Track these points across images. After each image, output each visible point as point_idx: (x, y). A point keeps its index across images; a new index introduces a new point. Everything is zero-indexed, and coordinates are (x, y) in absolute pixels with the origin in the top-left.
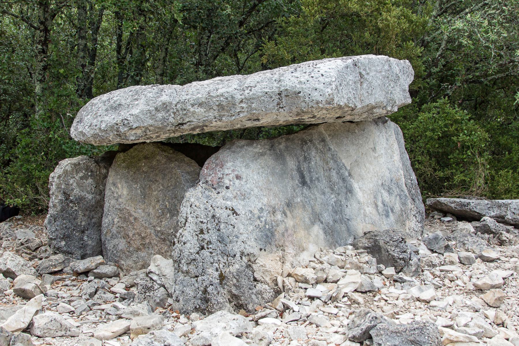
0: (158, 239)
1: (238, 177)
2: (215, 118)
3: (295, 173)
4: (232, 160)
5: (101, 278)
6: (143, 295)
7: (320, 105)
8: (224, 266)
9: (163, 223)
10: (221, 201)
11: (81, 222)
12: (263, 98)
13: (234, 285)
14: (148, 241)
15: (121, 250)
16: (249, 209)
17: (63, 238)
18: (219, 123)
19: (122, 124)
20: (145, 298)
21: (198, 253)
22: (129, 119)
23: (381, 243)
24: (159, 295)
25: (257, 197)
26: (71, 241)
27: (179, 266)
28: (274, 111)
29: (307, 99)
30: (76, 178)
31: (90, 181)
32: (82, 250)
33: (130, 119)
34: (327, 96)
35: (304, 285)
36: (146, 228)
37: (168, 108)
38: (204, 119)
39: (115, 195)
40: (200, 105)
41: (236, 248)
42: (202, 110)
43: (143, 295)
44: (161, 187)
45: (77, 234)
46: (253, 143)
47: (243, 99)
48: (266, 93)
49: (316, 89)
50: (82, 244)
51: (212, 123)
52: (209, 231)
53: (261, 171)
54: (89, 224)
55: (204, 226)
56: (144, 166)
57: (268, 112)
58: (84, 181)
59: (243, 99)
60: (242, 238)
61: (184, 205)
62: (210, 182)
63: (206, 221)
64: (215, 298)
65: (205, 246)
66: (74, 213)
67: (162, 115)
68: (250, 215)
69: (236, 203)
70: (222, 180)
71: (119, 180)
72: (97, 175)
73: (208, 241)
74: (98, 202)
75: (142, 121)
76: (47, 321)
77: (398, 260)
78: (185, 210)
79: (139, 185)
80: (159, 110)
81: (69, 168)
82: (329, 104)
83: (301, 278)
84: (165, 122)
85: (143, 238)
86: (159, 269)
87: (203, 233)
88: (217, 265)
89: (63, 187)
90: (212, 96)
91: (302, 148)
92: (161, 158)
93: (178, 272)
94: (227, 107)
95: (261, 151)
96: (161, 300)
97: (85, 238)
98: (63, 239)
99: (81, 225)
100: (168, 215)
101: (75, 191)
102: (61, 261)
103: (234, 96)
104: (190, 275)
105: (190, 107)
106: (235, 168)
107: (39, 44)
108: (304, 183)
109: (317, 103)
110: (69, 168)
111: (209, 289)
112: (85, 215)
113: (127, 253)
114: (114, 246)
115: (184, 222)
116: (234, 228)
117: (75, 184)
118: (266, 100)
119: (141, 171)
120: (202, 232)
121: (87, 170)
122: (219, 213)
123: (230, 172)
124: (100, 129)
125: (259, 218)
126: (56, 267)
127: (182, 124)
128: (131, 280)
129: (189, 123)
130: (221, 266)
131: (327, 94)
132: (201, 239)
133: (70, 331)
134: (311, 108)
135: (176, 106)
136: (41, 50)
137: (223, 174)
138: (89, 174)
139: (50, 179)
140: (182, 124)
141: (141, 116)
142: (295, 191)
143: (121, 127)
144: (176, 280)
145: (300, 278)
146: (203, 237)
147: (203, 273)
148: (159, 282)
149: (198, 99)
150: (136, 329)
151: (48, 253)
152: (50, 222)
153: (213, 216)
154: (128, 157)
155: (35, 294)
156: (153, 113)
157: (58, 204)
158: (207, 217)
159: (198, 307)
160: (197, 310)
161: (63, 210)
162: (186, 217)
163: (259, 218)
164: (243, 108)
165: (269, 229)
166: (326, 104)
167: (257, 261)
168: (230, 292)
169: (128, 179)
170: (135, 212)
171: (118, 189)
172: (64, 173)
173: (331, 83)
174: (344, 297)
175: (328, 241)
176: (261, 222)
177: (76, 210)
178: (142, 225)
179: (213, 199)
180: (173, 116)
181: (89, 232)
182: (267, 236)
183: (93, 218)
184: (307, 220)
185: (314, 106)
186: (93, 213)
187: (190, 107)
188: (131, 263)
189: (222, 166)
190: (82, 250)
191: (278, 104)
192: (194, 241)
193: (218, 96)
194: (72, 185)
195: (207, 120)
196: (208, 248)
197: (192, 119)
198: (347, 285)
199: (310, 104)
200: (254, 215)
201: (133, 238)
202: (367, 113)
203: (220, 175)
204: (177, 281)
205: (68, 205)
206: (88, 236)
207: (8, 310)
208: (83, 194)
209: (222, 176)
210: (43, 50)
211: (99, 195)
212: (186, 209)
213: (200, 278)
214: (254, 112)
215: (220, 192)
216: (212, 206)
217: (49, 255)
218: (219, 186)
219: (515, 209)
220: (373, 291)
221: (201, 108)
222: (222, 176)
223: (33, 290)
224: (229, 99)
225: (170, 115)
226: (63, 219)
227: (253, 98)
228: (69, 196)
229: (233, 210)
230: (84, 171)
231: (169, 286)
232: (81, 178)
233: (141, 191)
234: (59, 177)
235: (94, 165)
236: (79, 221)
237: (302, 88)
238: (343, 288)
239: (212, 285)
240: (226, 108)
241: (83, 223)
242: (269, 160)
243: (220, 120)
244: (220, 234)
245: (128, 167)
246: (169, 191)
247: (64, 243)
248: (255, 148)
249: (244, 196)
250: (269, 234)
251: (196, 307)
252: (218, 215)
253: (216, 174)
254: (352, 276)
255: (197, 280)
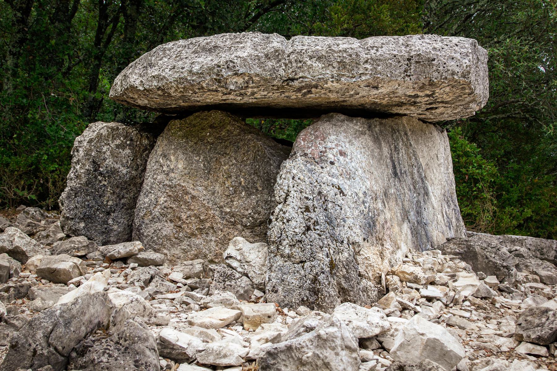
0: (224, 222)
1: (342, 153)
2: (333, 78)
3: (388, 161)
4: (335, 133)
5: (146, 265)
6: (222, 285)
7: (456, 77)
8: (334, 252)
9: (235, 203)
10: (326, 176)
11: (108, 201)
12: (390, 61)
13: (344, 276)
14: (208, 225)
15: (166, 235)
16: (355, 190)
17: (83, 219)
18: (335, 84)
19: (226, 67)
20: (225, 287)
21: (304, 234)
22: (236, 61)
23: (478, 249)
24: (243, 286)
25: (361, 178)
26: (92, 223)
27: (278, 249)
28: (399, 79)
29: (441, 68)
30: (111, 145)
31: (128, 151)
32: (104, 236)
33: (238, 61)
34: (465, 68)
35: (414, 285)
36: (208, 209)
37: (280, 57)
38: (320, 77)
39: (165, 168)
40: (319, 58)
41: (343, 233)
42: (320, 65)
43: (222, 285)
44: (234, 161)
45: (101, 216)
46: (353, 120)
47: (368, 59)
48: (395, 56)
49: (453, 59)
50: (106, 229)
51: (327, 83)
52: (315, 209)
53: (363, 150)
54: (117, 205)
55: (310, 203)
56: (210, 136)
57: (393, 79)
58: (121, 150)
59: (368, 59)
60: (350, 222)
61: (283, 176)
62: (310, 156)
63: (312, 198)
64: (326, 289)
65: (312, 227)
66: (101, 188)
67: (272, 64)
68: (356, 198)
69: (342, 182)
70: (325, 154)
71: (172, 151)
72: (136, 145)
73: (315, 221)
74: (132, 179)
75: (249, 67)
76: (125, 302)
77: (502, 268)
78: (284, 182)
79: (202, 157)
80: (269, 58)
81: (104, 132)
82: (464, 77)
83: (409, 277)
84: (275, 73)
85: (202, 221)
86: (242, 254)
87: (309, 212)
88: (327, 249)
89: (93, 154)
90: (334, 51)
91: (392, 136)
92: (232, 127)
93: (276, 256)
94: (349, 65)
95: (361, 130)
96: (246, 292)
97: (110, 222)
98: (82, 219)
99: (107, 205)
100: (243, 193)
101: (107, 161)
102: (85, 244)
103: (359, 53)
104: (293, 259)
105: (308, 60)
106: (339, 142)
107: (19, 12)
108: (395, 174)
109: (453, 74)
110: (104, 132)
111: (321, 277)
112: (114, 193)
113: (174, 240)
114: (155, 231)
115: (284, 197)
116: (341, 209)
117: (108, 153)
118: (393, 63)
119: (206, 141)
120: (307, 209)
121: (126, 137)
122: (326, 189)
123: (334, 147)
124: (191, 72)
125: (364, 202)
126: (79, 251)
127: (293, 80)
128: (188, 270)
129: (301, 79)
130: (332, 252)
131: (465, 65)
132: (307, 217)
133: (155, 317)
134: (444, 79)
135: (289, 56)
136: (21, 19)
137: (325, 148)
138: (128, 142)
139: (76, 144)
140: (293, 80)
141: (249, 60)
142: (389, 180)
143: (224, 70)
144: (272, 266)
145: (407, 276)
146: (310, 216)
147: (313, 257)
148: (240, 270)
149: (317, 51)
150: (254, 316)
151: (51, 239)
152: (68, 197)
153: (320, 193)
154: (187, 125)
155: (73, 276)
156: (263, 60)
157: (83, 175)
158: (313, 193)
159: (305, 299)
160: (303, 302)
161: (87, 184)
162: (288, 191)
163: (364, 202)
164: (367, 70)
165: (372, 218)
166: (462, 76)
167: (361, 252)
168: (339, 284)
169: (186, 150)
170: (194, 190)
171: (171, 161)
172: (97, 137)
173: (468, 54)
174: (463, 301)
175: (414, 243)
176: (365, 208)
177: (104, 185)
178: (204, 206)
179: (318, 174)
180: (284, 67)
181: (116, 214)
182: (370, 225)
183: (123, 197)
184: (399, 215)
185: (448, 77)
186: (125, 191)
187: (308, 60)
188: (177, 252)
189: (324, 139)
190: (104, 236)
191: (406, 71)
192: (300, 219)
193: (340, 51)
194: (104, 153)
195: (323, 78)
196: (315, 230)
197: (306, 74)
198: (465, 287)
199: (444, 74)
200: (359, 198)
201: (187, 221)
202: (462, 107)
203: (321, 148)
204: (274, 268)
205: (96, 177)
206: (113, 220)
207: (47, 290)
208: (117, 166)
209: (324, 150)
210: (23, 18)
211: (136, 170)
212: (286, 181)
213: (307, 264)
214: (379, 76)
215: (324, 167)
216: (317, 181)
217: (52, 241)
218: (322, 161)
219: (530, 245)
220: (489, 298)
221: (319, 62)
222: (324, 150)
223: (71, 270)
224: (354, 56)
225: (281, 66)
226: (87, 195)
227: (380, 60)
228: (99, 167)
229: (339, 188)
230: (122, 139)
231: (254, 275)
232: (118, 146)
233: (204, 164)
234: (90, 141)
235: (135, 132)
236: (106, 198)
237: (437, 55)
238: (462, 290)
239: (323, 273)
240: (348, 66)
241: (110, 203)
242: (367, 140)
243: (338, 81)
244: (328, 214)
245: (186, 136)
246: (246, 166)
247: (83, 225)
248: (356, 125)
249: (350, 176)
250: (372, 223)
251: (303, 300)
252: (325, 192)
253: (316, 147)
254: (466, 279)
255: (303, 267)
